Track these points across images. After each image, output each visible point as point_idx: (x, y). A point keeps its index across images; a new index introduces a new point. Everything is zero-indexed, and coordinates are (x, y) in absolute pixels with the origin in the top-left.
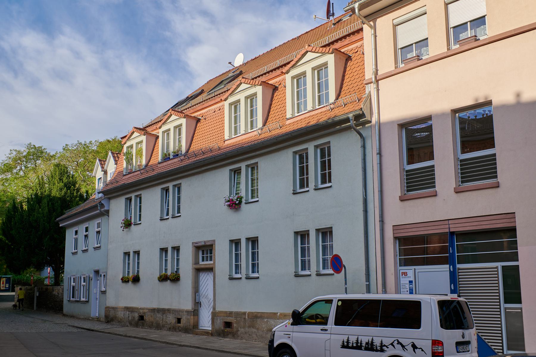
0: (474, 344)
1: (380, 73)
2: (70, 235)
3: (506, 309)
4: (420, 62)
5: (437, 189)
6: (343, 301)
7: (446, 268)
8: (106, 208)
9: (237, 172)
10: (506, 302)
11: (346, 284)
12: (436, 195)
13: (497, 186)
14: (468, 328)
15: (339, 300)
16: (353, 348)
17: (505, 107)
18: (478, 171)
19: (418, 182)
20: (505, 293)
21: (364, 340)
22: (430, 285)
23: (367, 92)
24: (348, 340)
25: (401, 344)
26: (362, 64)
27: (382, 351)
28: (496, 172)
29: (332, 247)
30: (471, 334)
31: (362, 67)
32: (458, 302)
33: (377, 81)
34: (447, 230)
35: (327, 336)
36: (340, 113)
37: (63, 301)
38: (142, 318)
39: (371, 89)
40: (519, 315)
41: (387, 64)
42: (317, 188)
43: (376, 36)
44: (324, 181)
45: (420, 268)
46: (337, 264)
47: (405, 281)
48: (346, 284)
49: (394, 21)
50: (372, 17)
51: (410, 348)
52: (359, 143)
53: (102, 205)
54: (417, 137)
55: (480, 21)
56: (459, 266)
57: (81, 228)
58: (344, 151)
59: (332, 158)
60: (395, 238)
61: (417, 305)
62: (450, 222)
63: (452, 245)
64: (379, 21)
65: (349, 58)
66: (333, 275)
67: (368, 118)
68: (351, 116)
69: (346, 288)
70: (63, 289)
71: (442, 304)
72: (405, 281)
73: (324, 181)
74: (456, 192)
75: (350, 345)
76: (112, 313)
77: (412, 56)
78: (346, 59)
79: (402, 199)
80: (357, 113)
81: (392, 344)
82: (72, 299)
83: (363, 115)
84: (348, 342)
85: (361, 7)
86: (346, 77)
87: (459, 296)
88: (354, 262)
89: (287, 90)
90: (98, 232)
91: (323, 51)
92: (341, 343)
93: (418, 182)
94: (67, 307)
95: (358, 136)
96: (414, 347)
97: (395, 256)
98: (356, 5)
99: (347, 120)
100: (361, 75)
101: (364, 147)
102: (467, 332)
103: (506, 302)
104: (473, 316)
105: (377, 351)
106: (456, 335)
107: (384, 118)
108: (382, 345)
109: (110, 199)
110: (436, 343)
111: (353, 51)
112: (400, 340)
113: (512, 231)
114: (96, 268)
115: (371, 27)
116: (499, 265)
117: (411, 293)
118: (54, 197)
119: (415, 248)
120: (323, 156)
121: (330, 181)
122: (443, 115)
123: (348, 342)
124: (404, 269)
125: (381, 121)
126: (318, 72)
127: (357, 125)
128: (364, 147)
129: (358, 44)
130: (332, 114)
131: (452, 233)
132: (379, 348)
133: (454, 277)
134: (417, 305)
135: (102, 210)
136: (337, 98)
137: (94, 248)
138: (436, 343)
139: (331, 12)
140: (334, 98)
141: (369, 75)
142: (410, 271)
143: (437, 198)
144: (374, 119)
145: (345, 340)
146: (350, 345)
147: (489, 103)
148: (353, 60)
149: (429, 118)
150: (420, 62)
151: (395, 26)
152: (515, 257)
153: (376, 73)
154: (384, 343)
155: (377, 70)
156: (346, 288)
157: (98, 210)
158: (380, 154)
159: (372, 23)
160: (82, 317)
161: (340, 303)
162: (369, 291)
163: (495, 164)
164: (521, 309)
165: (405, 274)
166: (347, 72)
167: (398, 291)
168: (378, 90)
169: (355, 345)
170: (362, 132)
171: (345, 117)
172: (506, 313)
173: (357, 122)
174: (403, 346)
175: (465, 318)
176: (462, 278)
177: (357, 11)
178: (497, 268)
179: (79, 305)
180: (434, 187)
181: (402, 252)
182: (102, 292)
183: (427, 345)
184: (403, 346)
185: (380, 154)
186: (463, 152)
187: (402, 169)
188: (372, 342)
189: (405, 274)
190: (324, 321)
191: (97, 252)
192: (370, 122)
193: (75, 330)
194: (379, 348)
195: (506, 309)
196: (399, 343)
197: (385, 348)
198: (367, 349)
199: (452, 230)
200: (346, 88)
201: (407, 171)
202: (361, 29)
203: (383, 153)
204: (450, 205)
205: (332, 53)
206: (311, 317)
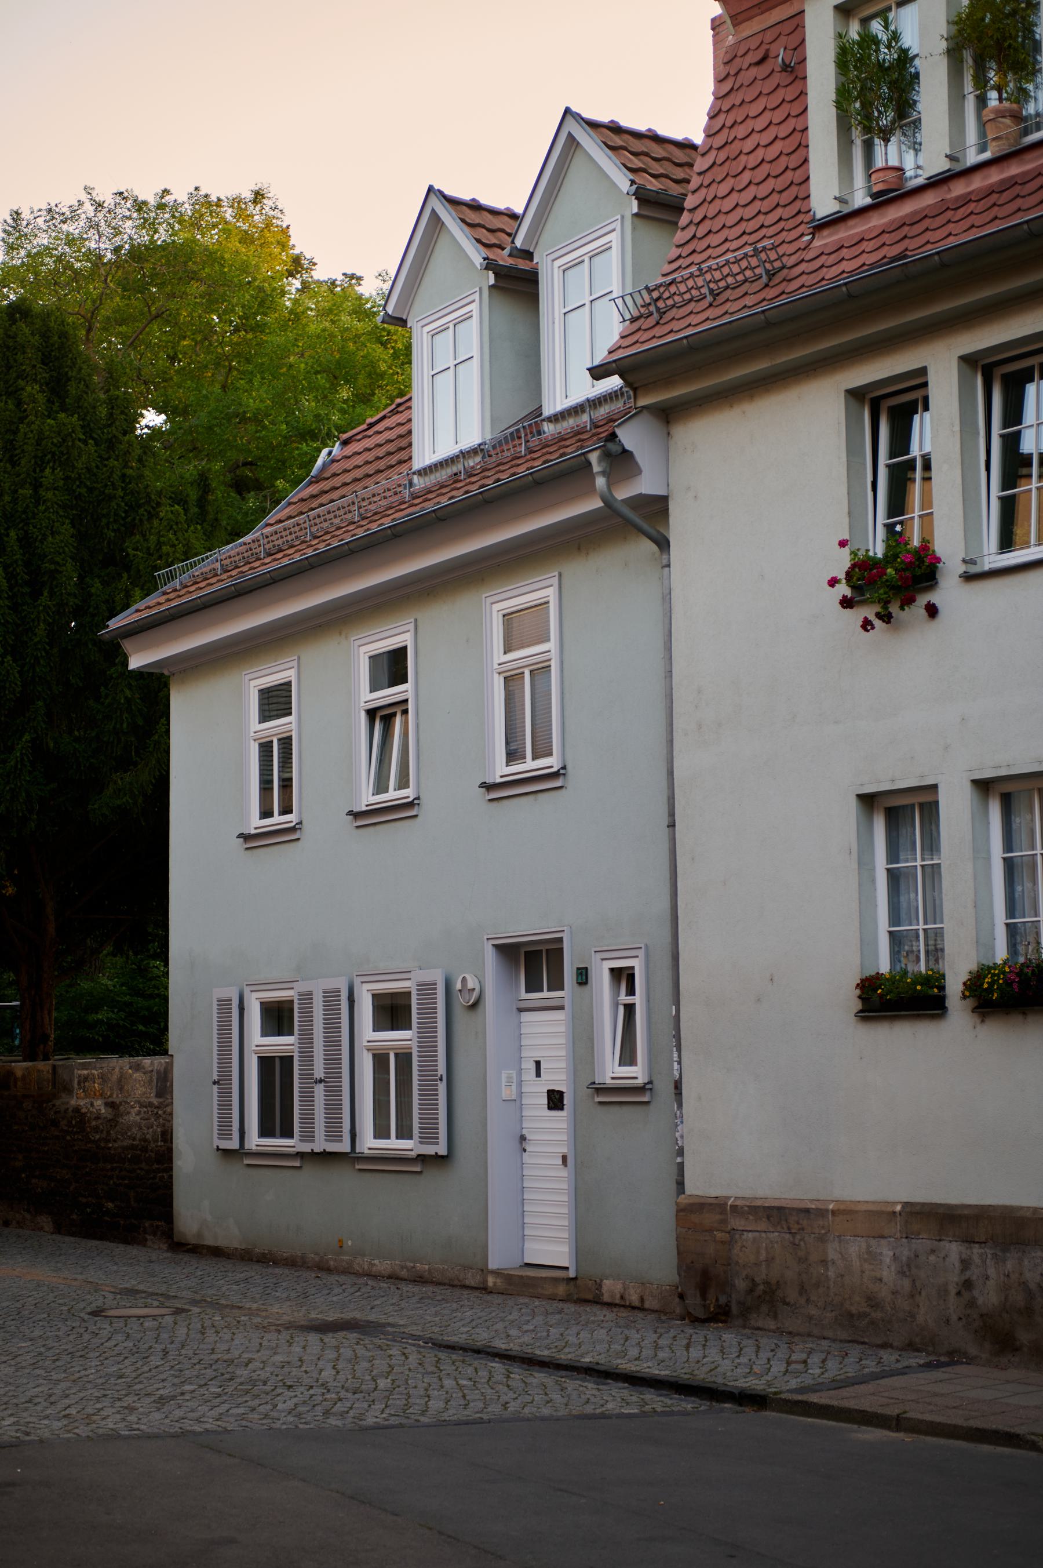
2: (210, 743)
8: (646, 485)
9: (895, 408)
31: (798, 176)
37: (165, 1157)
42: (974, 569)
53: (621, 461)
57: (336, 680)
70: (164, 1084)
76: (756, 1249)
82: (254, 1141)
89: (812, 132)
90: (382, 717)
94: (203, 1195)
109: (668, 415)
114: (527, 927)
118: (1034, 32)
135: (622, 494)
137: (356, 815)
157: (592, 490)
160: (382, 1266)
179: (343, 1182)
182: (601, 1090)
191: (523, 812)
193: (615, 1399)
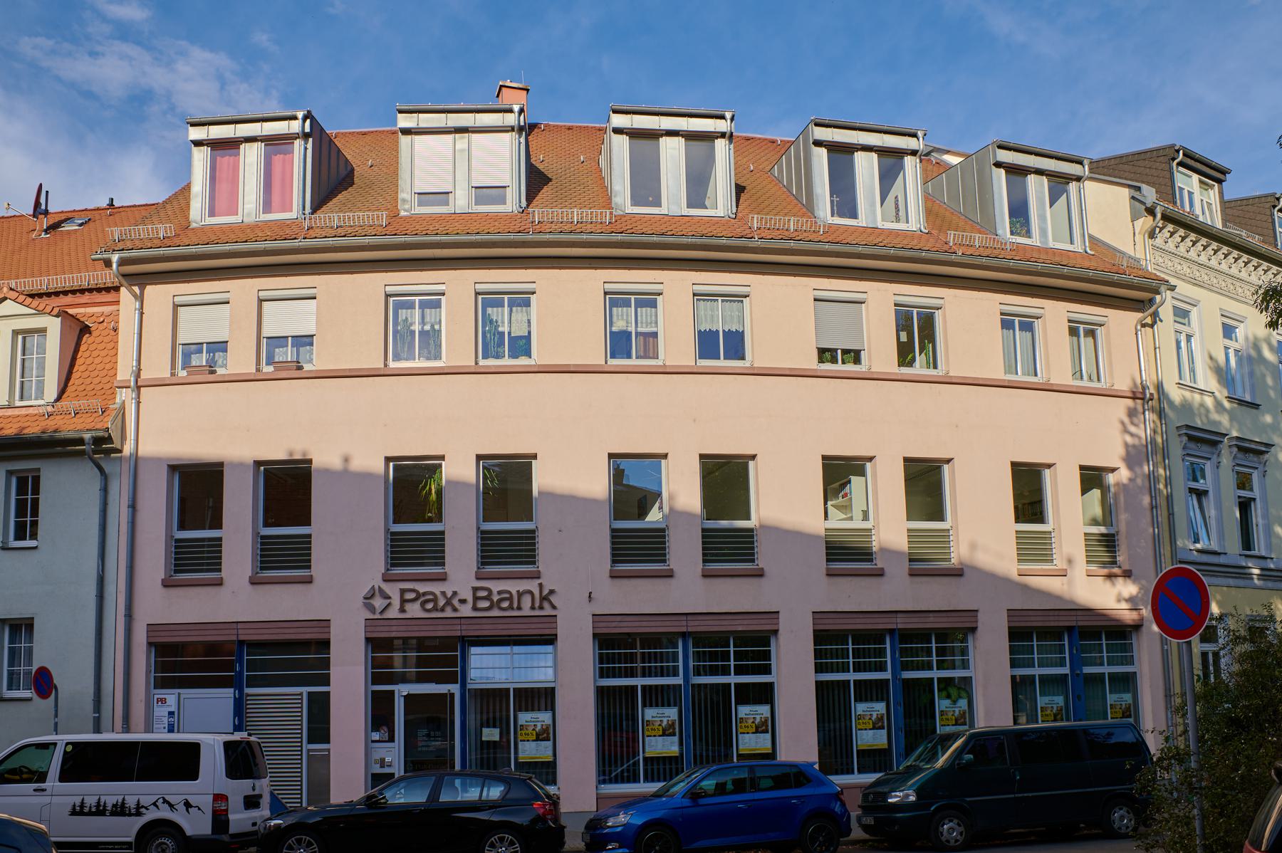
0: (266, 800)
1: (144, 375)
3: (309, 751)
4: (211, 377)
5: (223, 574)
6: (76, 745)
7: (228, 693)
10: (310, 742)
11: (56, 716)
12: (221, 584)
13: (309, 581)
14: (259, 778)
15: (67, 744)
16: (90, 813)
17: (327, 472)
18: (284, 557)
19: (194, 562)
20: (309, 729)
21: (110, 801)
22: (205, 719)
23: (118, 400)
24: (82, 802)
25: (168, 803)
26: (112, 352)
27: (139, 814)
28: (309, 561)
29: (30, 652)
30: (263, 786)
32: (248, 743)
33: (139, 388)
34: (234, 638)
35: (47, 799)
36: (68, 427)
38: (1177, 710)
39: (125, 396)
40: (326, 759)
41: (157, 366)
43: (142, 314)
44: (20, 535)
45: (186, 693)
46: (43, 683)
47: (161, 712)
48: (56, 716)
49: (177, 299)
50: (141, 279)
51: (181, 807)
52: (97, 485)
54: (198, 486)
55: (304, 341)
56: (248, 691)
58: (66, 491)
59: (42, 497)
60: (150, 644)
61: (194, 748)
62: (240, 626)
63: (240, 661)
64: (149, 289)
65: (85, 330)
66: (30, 700)
67: (117, 445)
68: (87, 436)
69: (56, 724)
71: (228, 746)
72: (161, 712)
73: (20, 535)
74: (252, 583)
75: (86, 810)
77: (200, 363)
78: (78, 331)
79: (167, 584)
80: (101, 434)
81: (155, 804)
83: (109, 439)
84: (82, 805)
85: (122, 262)
86: (79, 362)
87: (250, 735)
88: (73, 679)
91: (41, 308)
92: (70, 808)
93: (194, 562)
95: (96, 470)
96: (188, 805)
97: (148, 672)
98: (115, 258)
99: (81, 441)
100: (108, 367)
101: (105, 490)
102: (258, 783)
103: (310, 742)
104: (268, 761)
105: (130, 815)
106: (243, 787)
107: (146, 449)
108: (139, 806)
110: (219, 798)
111: (94, 319)
112: (167, 798)
113: (325, 645)
115: (135, 296)
116: (305, 690)
117: (171, 730)
119: (185, 660)
120: (21, 489)
121: (34, 536)
122: (240, 465)
123: (82, 805)
124: (161, 694)
125: (140, 453)
126: (24, 339)
127: (95, 452)
128: (105, 490)
129: (107, 309)
130: (51, 424)
131: (241, 643)
132: (133, 811)
133: (239, 707)
134: (194, 748)
136: (59, 399)
138: (219, 798)
139: (43, 207)
140: (55, 396)
141: (124, 372)
142: (171, 696)
143: (222, 589)
144: (128, 449)
145: (78, 803)
146: (86, 810)
147: (310, 461)
148: (94, 334)
149: (221, 464)
150: (211, 377)
151: (176, 307)
152: (326, 680)
153: (138, 376)
154: (142, 803)
155: (139, 370)
156: (56, 724)
158: (133, 506)
159: (136, 289)
161: (70, 748)
162: (97, 730)
163: (310, 549)
164: (329, 750)
165: (163, 701)
166: (80, 354)
167: (149, 729)
168: (139, 403)
169: (94, 809)
170: (103, 465)
171: (76, 436)
172: (309, 756)
173: (100, 449)
174: (171, 806)
175: (256, 765)
176: (250, 705)
177: (114, 266)
178: (301, 694)
180: (220, 570)
181: (161, 667)
183: (206, 802)
184: (171, 806)
185: (133, 506)
186: (266, 525)
187: (169, 536)
188: (123, 803)
189: (163, 701)
190: (42, 777)
192: (120, 451)
194: (133, 811)
195: (309, 751)
196: (165, 801)
197: (143, 810)
198: (113, 814)
199: (241, 638)
200: (77, 382)
201: (177, 541)
202: (117, 289)
203: (140, 505)
204: (237, 600)
205: (57, 316)
206: (13, 771)
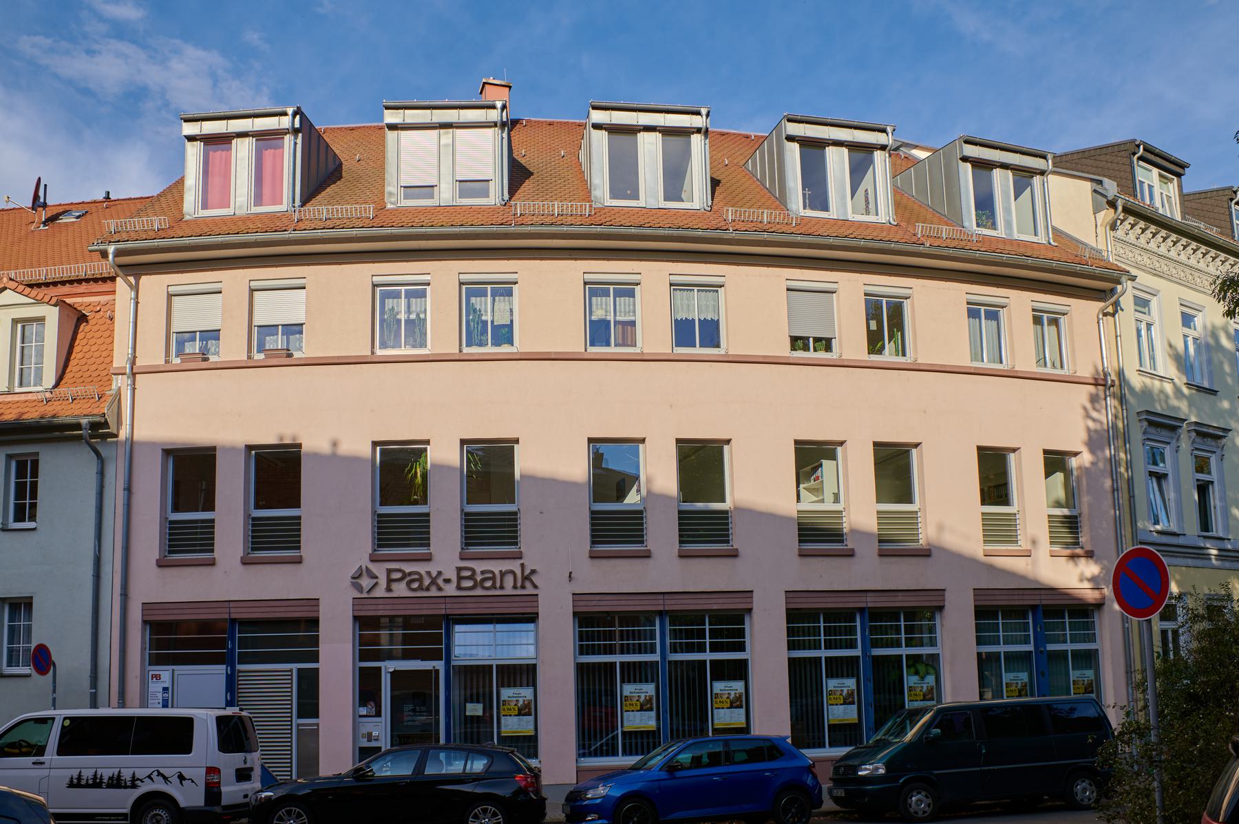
0: (257, 773)
1: (139, 362)
3: (298, 725)
4: (204, 365)
5: (216, 554)
6: (73, 720)
7: (221, 669)
10: (299, 717)
11: (54, 691)
12: (213, 564)
13: (299, 561)
14: (250, 751)
15: (65, 719)
16: (87, 786)
17: (316, 456)
18: (274, 538)
19: (187, 542)
20: (299, 704)
21: (107, 774)
22: (198, 695)
23: (114, 387)
24: (80, 775)
25: (163, 776)
26: (109, 340)
27: (134, 786)
28: (299, 542)
29: (29, 629)
30: (255, 759)
32: (240, 718)
33: (134, 374)
34: (226, 616)
35: (46, 772)
36: (66, 412)
38: (1138, 686)
39: (120, 382)
40: (315, 733)
41: (152, 354)
43: (137, 303)
44: (19, 517)
45: (180, 669)
46: (42, 660)
47: (156, 688)
48: (54, 691)
49: (171, 289)
50: (136, 270)
51: (175, 780)
52: (94, 468)
54: (192, 470)
55: (294, 329)
56: (239, 667)
58: (64, 474)
59: (40, 480)
60: (145, 622)
61: (188, 723)
62: (232, 605)
63: (232, 638)
64: (144, 279)
65: (82, 318)
66: (29, 676)
67: (113, 429)
68: (84, 421)
69: (54, 699)
71: (220, 720)
72: (156, 688)
73: (19, 517)
74: (244, 564)
75: (83, 782)
77: (194, 350)
78: (76, 320)
79: (161, 564)
80: (97, 419)
81: (149, 777)
83: (105, 424)
84: (79, 777)
85: (118, 253)
86: (76, 349)
87: (241, 710)
88: (71, 656)
91: (39, 297)
92: (67, 781)
93: (187, 542)
95: (93, 454)
96: (181, 777)
97: (143, 649)
98: (111, 249)
99: (78, 426)
100: (104, 354)
101: (101, 473)
102: (249, 756)
103: (299, 717)
104: (259, 735)
105: (126, 787)
106: (235, 760)
107: (141, 434)
108: (134, 779)
110: (212, 770)
111: (90, 308)
112: (162, 771)
113: (314, 623)
115: (130, 285)
116: (295, 666)
117: (165, 705)
119: (179, 638)
120: (21, 473)
121: (33, 518)
122: (232, 450)
123: (79, 777)
124: (155, 670)
125: (135, 438)
126: (23, 327)
127: (92, 437)
128: (101, 473)
129: (103, 299)
130: (49, 410)
131: (233, 621)
132: (129, 784)
133: (231, 683)
134: (188, 723)
136: (57, 385)
138: (212, 770)
139: (42, 200)
140: (53, 382)
141: (120, 360)
142: (165, 673)
143: (215, 569)
144: (123, 434)
145: (75, 776)
146: (83, 782)
147: (300, 446)
148: (91, 322)
149: (214, 449)
150: (204, 365)
151: (170, 296)
152: (315, 657)
153: (133, 363)
154: (137, 776)
155: (135, 357)
156: (54, 699)
158: (129, 489)
159: (132, 279)
161: (67, 723)
162: (94, 705)
163: (299, 530)
164: (318, 725)
165: (158, 677)
166: (77, 342)
167: (144, 704)
168: (134, 389)
169: (90, 782)
170: (100, 449)
171: (74, 421)
172: (298, 730)
173: (97, 434)
174: (165, 778)
175: (247, 739)
176: (242, 681)
177: (111, 257)
178: (291, 671)
180: (212, 551)
181: (155, 644)
183: (200, 775)
184: (165, 778)
185: (129, 489)
186: (257, 507)
187: (163, 518)
188: (119, 776)
189: (158, 677)
190: (40, 751)
192: (116, 436)
194: (129, 784)
195: (298, 725)
196: (160, 774)
197: (138, 783)
198: (109, 786)
199: (233, 616)
200: (75, 369)
201: (171, 522)
202: (113, 279)
203: (135, 488)
204: (229, 579)
205: (55, 305)
206: (12, 745)
